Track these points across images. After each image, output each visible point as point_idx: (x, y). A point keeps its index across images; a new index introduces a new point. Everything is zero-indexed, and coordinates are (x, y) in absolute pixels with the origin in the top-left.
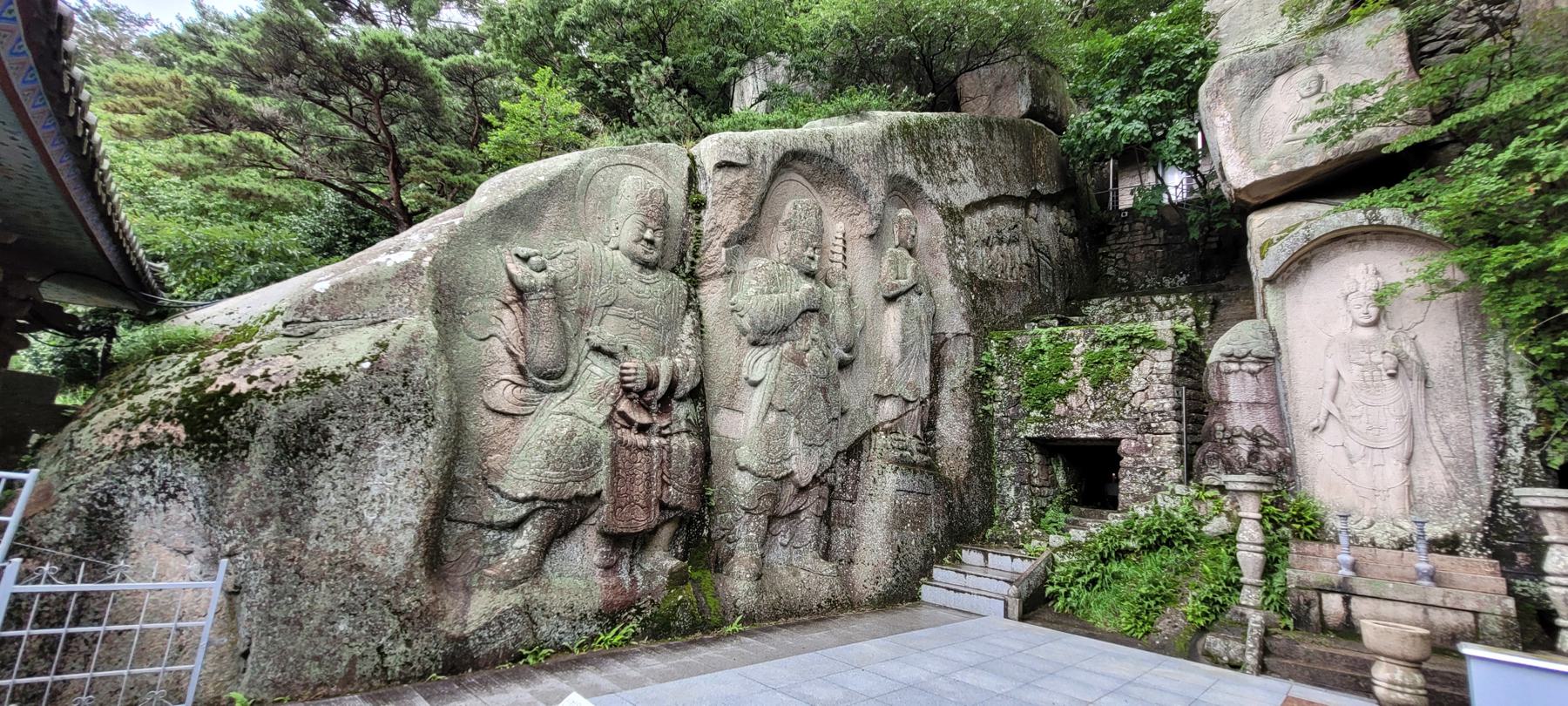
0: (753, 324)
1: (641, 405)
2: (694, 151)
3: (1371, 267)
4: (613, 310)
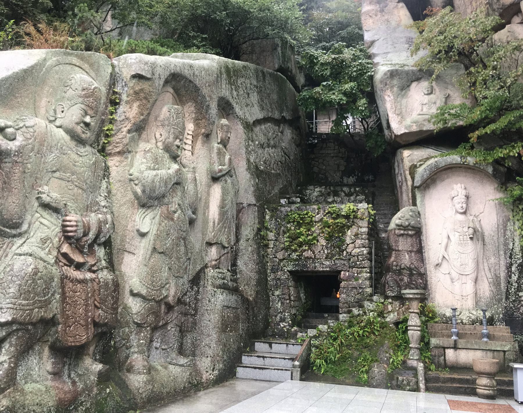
0: (144, 191)
1: (77, 248)
2: (115, 62)
3: (463, 185)
4: (57, 174)
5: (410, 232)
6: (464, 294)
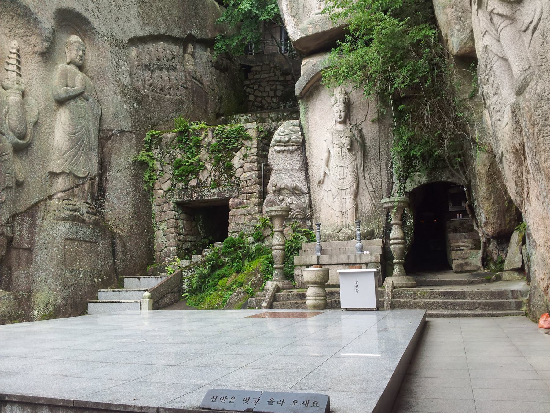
5: (291, 148)
6: (344, 210)
